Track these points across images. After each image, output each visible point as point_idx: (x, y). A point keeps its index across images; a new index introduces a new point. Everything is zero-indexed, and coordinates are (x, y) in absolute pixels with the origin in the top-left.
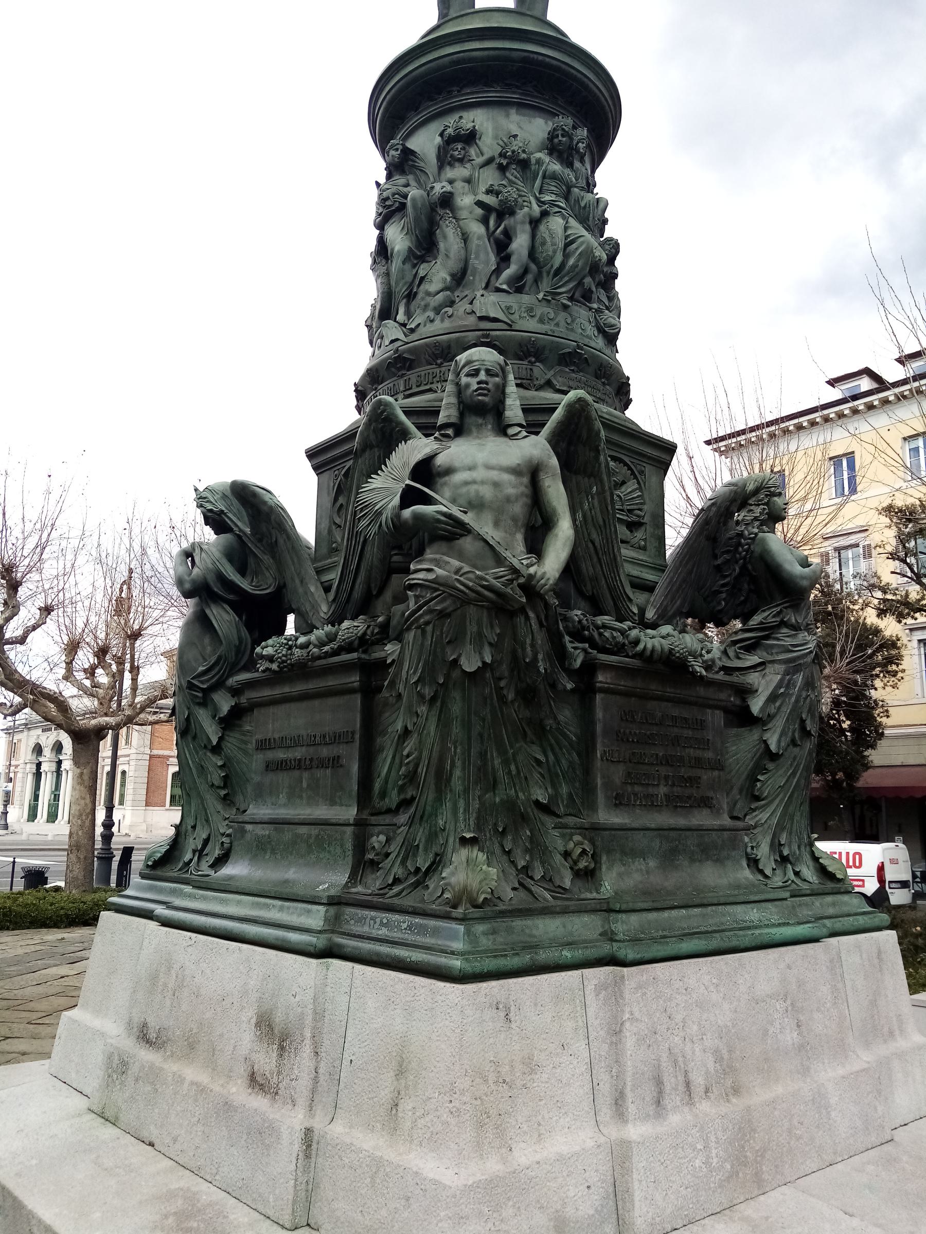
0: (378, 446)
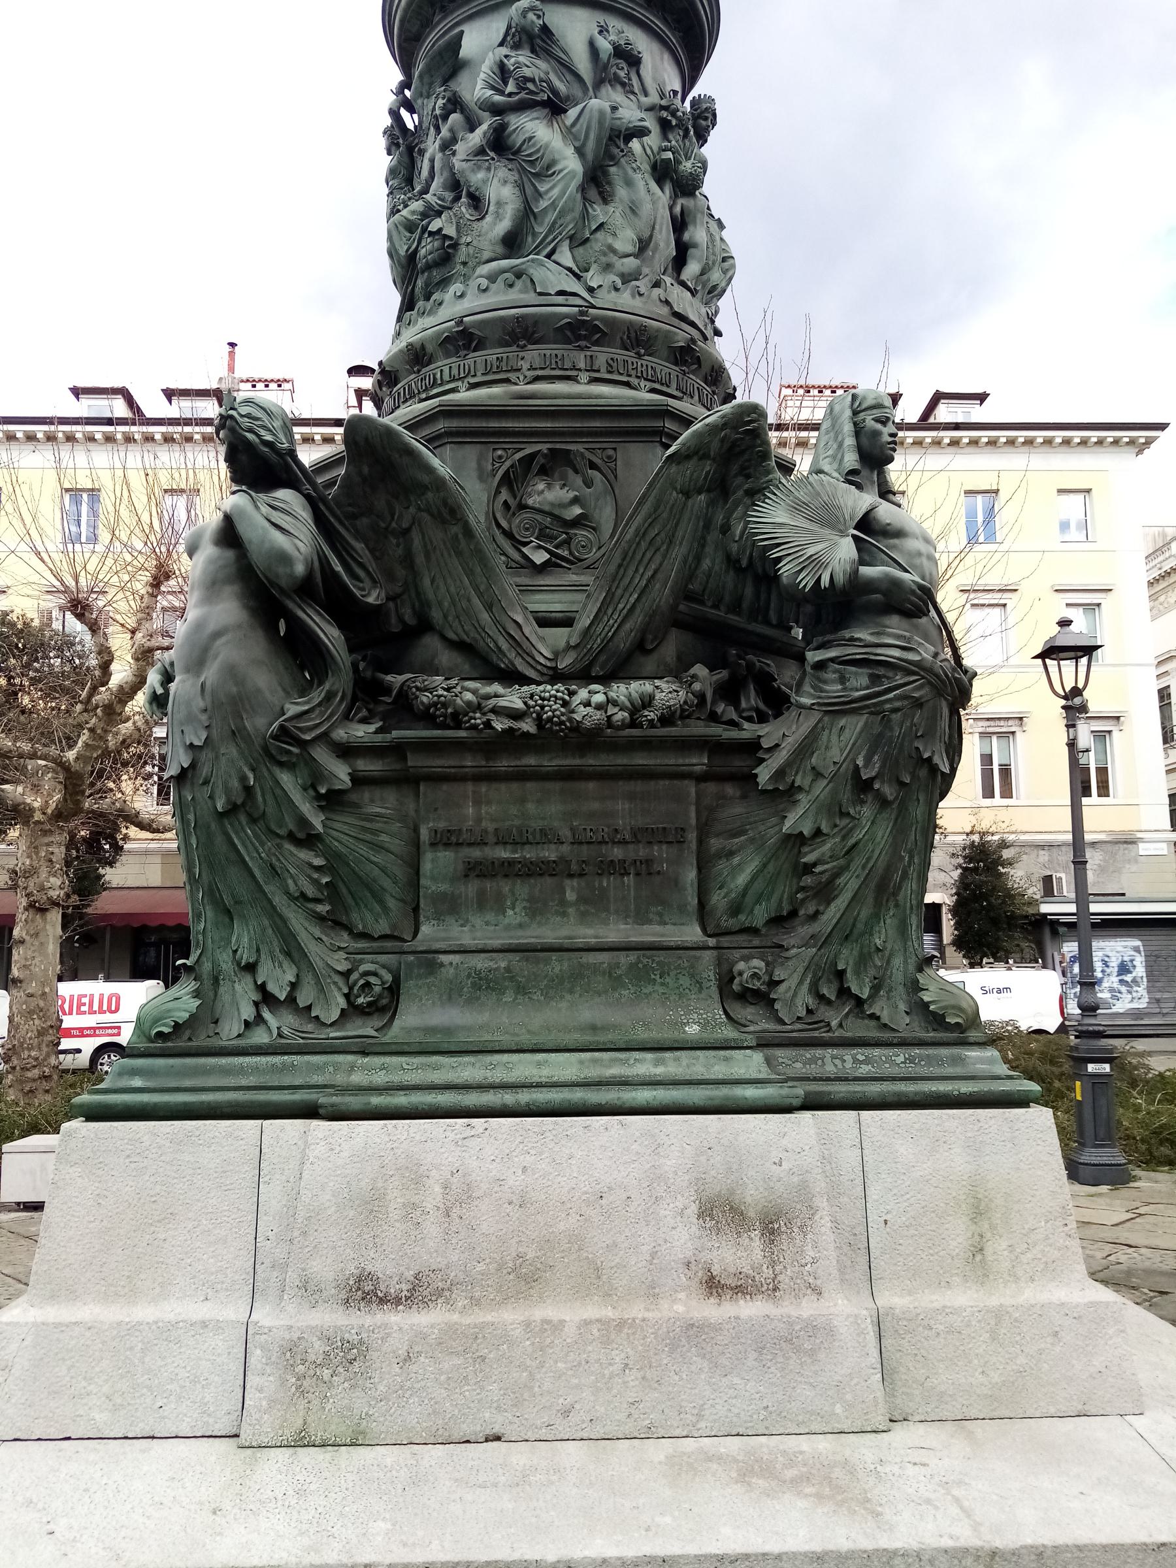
0: (714, 460)
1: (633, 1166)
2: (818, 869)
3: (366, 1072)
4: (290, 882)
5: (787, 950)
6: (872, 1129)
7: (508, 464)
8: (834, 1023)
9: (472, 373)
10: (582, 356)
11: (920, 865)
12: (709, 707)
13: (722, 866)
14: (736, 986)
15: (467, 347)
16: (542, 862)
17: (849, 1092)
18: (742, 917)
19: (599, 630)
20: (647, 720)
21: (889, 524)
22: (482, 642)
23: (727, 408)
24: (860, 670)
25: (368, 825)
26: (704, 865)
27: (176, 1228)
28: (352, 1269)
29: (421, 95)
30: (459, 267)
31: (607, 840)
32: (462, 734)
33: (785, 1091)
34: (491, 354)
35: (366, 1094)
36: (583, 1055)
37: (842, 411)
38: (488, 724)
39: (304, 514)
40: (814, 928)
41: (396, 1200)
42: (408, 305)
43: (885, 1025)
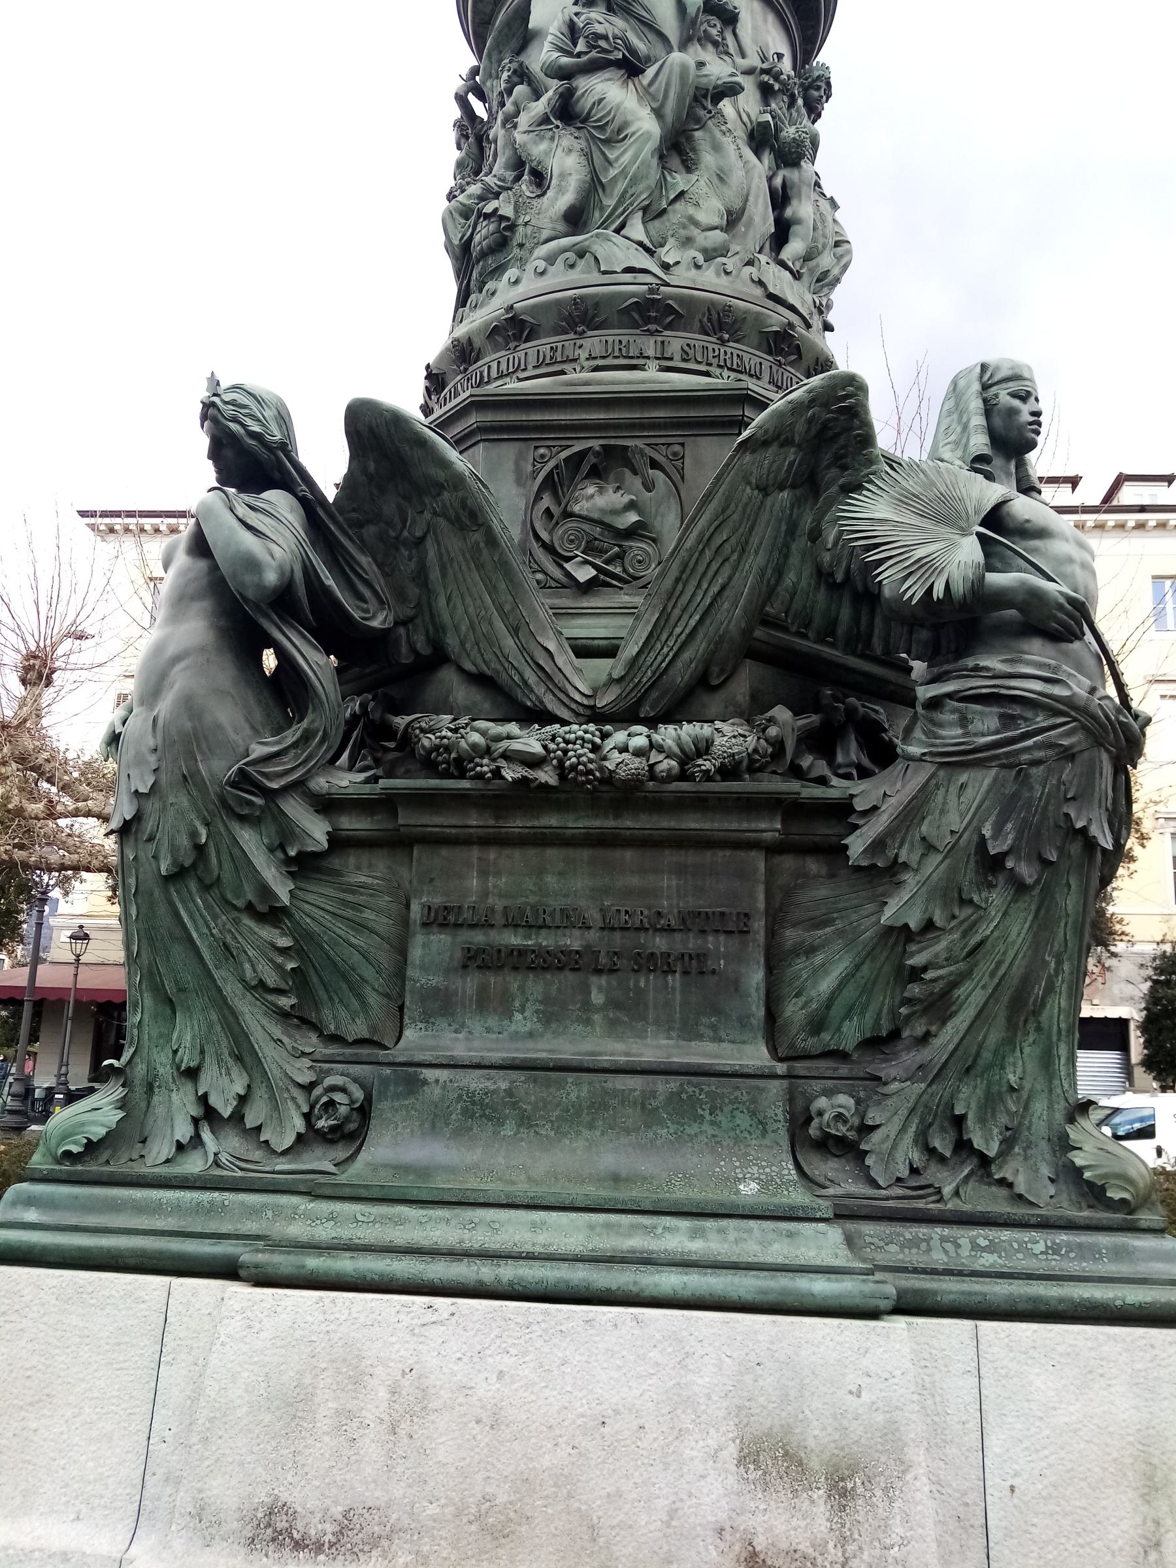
0: (799, 446)
1: (650, 1382)
2: (929, 975)
3: (309, 1222)
4: (247, 966)
5: (886, 1084)
6: (995, 1350)
7: (551, 464)
8: (947, 1190)
9: (523, 367)
10: (652, 342)
11: (1071, 973)
12: (789, 757)
13: (800, 966)
14: (813, 1131)
15: (518, 338)
16: (562, 952)
17: (963, 1293)
18: (826, 1036)
19: (650, 660)
20: (701, 771)
21: (1028, 521)
22: (504, 675)
23: (816, 380)
24: (987, 709)
25: (350, 898)
26: (774, 963)
27: (52, 1416)
28: (262, 1496)
29: (491, 76)
30: (516, 251)
31: (647, 926)
32: (465, 784)
33: (869, 1288)
34: (543, 345)
35: (302, 1253)
36: (594, 1217)
37: (968, 386)
38: (497, 773)
39: (291, 517)
40: (924, 1055)
41: (327, 1405)
42: (463, 300)
43: (1020, 1196)
